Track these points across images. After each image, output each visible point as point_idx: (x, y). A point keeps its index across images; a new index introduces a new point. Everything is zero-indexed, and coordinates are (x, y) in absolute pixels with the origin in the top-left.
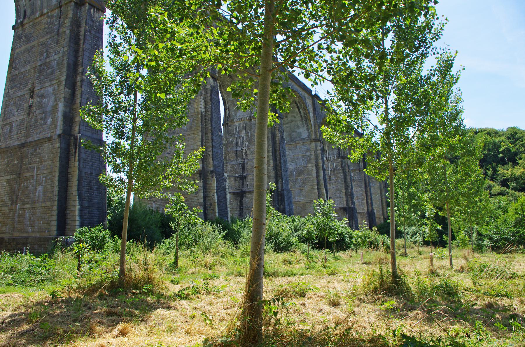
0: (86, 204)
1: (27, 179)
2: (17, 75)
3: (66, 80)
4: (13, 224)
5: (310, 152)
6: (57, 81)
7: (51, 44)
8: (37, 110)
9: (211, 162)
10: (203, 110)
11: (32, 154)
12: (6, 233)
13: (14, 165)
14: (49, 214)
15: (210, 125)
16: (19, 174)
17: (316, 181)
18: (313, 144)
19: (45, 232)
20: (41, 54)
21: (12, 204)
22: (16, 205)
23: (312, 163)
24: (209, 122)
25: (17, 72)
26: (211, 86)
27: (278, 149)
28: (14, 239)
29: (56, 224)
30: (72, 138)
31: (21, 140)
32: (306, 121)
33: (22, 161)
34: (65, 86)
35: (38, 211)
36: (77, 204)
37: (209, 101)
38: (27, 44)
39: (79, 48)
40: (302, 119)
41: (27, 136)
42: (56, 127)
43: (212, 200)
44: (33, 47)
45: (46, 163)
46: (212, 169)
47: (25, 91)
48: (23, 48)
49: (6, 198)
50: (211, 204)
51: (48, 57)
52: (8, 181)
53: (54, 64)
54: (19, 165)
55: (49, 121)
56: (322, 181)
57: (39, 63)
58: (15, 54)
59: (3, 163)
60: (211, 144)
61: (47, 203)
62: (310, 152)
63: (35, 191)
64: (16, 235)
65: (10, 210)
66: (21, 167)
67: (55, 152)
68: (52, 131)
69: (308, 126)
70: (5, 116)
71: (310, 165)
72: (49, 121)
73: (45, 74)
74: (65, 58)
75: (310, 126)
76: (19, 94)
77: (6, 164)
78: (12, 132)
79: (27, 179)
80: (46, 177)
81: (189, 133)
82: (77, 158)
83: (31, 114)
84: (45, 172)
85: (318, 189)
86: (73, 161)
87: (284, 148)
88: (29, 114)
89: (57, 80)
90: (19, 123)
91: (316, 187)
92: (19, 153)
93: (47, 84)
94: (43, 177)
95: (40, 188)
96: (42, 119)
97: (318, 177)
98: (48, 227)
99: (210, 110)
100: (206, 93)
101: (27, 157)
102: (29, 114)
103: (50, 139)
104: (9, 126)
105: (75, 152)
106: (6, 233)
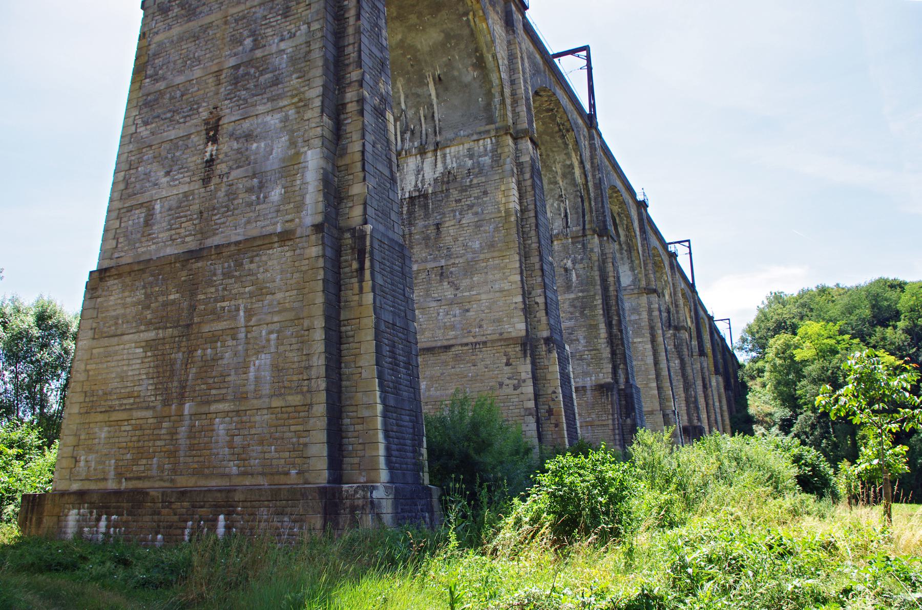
0: (392, 402)
1: (214, 339)
2: (161, 93)
3: (324, 95)
4: (172, 454)
5: (639, 314)
6: (296, 100)
7: (265, 17)
8: (231, 168)
9: (544, 319)
10: (518, 208)
11: (227, 275)
12: (148, 478)
13: (165, 305)
14: (300, 428)
15: (534, 239)
16: (188, 326)
17: (653, 372)
18: (644, 299)
19: (287, 474)
20: (237, 41)
21: (166, 403)
22: (182, 404)
23: (643, 336)
24: (533, 233)
25: (161, 85)
26: (532, 158)
27: (613, 302)
28: (183, 494)
29: (325, 454)
30: (348, 235)
31: (183, 242)
32: (629, 251)
33: (193, 294)
34: (322, 112)
35: (258, 418)
36: (378, 401)
37: (529, 189)
38: (189, 20)
39: (345, 28)
40: (621, 249)
41: (203, 234)
42: (300, 207)
43: (551, 404)
44: (205, 28)
45: (279, 296)
46: (546, 334)
47: (195, 124)
48: (176, 31)
49: (146, 388)
50: (550, 412)
51: (256, 46)
52: (149, 345)
53: (282, 62)
54: (185, 305)
55: (276, 194)
56: (665, 373)
57: (232, 62)
58: (153, 46)
59: (129, 300)
60: (539, 279)
61: (290, 398)
62: (639, 314)
63: (244, 367)
64: (185, 482)
65: (160, 419)
66: (193, 308)
67: (304, 268)
68: (289, 217)
69: (632, 261)
70: (126, 188)
71: (639, 340)
72: (276, 194)
73: (251, 85)
74: (316, 45)
75: (637, 262)
76: (172, 134)
77: (139, 303)
78: (152, 225)
79: (214, 339)
80: (278, 332)
81: (488, 256)
82: (368, 285)
83: (215, 180)
84: (276, 319)
85: (659, 388)
86: (356, 290)
87: (622, 300)
88: (206, 181)
89: (293, 96)
90: (174, 203)
91: (655, 384)
92: (184, 273)
93: (261, 109)
94: (271, 332)
95: (264, 360)
96: (250, 190)
97: (656, 363)
98: (298, 461)
99: (532, 207)
100: (521, 172)
101: (210, 283)
102: (206, 181)
103: (286, 237)
104: (144, 210)
105: (362, 269)
106: (148, 478)
